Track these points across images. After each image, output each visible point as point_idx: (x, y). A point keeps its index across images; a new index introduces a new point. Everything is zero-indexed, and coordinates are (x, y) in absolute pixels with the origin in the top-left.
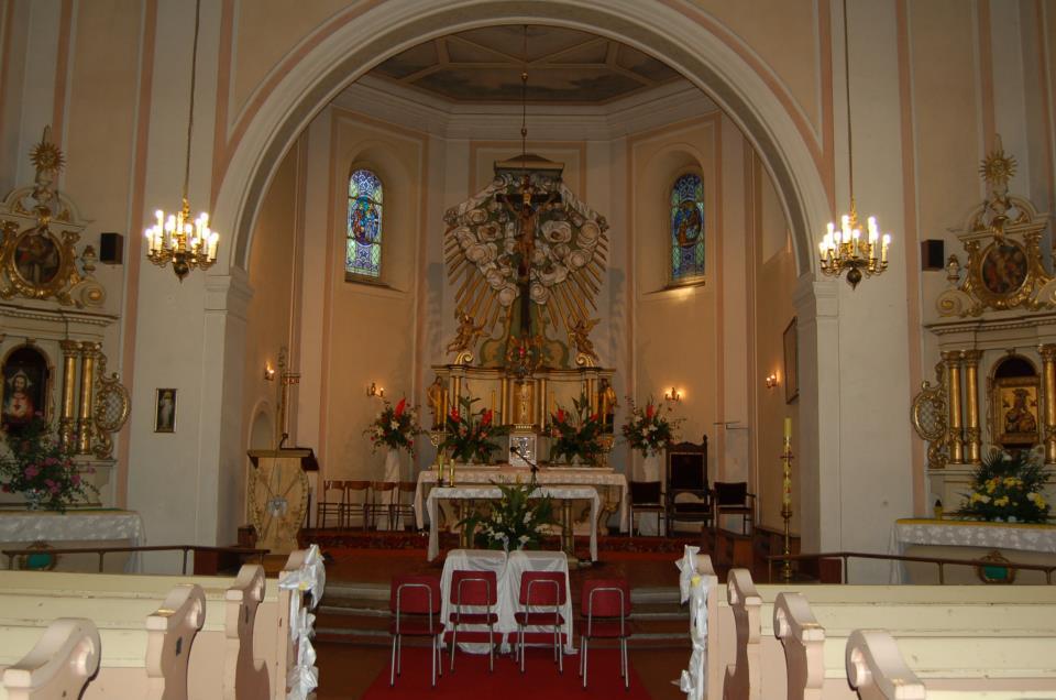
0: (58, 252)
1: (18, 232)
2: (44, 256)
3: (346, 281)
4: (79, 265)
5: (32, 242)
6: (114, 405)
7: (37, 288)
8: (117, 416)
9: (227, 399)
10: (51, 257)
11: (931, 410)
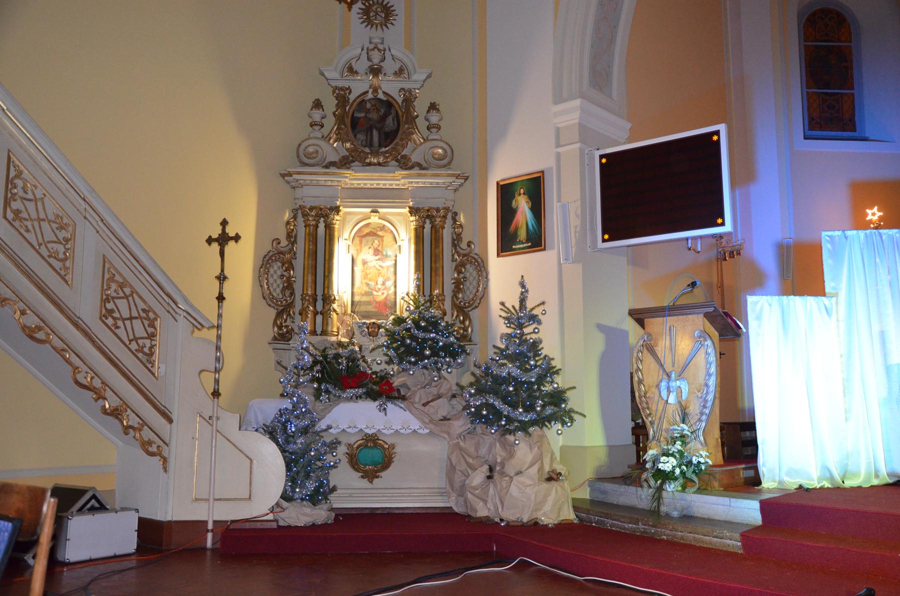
0: (397, 112)
1: (352, 97)
2: (383, 118)
3: (805, 138)
4: (421, 123)
5: (368, 106)
6: (471, 279)
7: (376, 154)
8: (474, 291)
9: (747, 315)
10: (390, 120)
11: (279, 273)
